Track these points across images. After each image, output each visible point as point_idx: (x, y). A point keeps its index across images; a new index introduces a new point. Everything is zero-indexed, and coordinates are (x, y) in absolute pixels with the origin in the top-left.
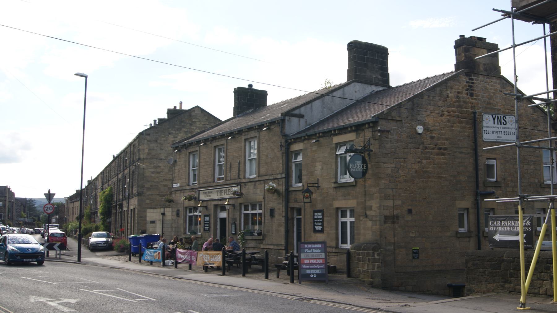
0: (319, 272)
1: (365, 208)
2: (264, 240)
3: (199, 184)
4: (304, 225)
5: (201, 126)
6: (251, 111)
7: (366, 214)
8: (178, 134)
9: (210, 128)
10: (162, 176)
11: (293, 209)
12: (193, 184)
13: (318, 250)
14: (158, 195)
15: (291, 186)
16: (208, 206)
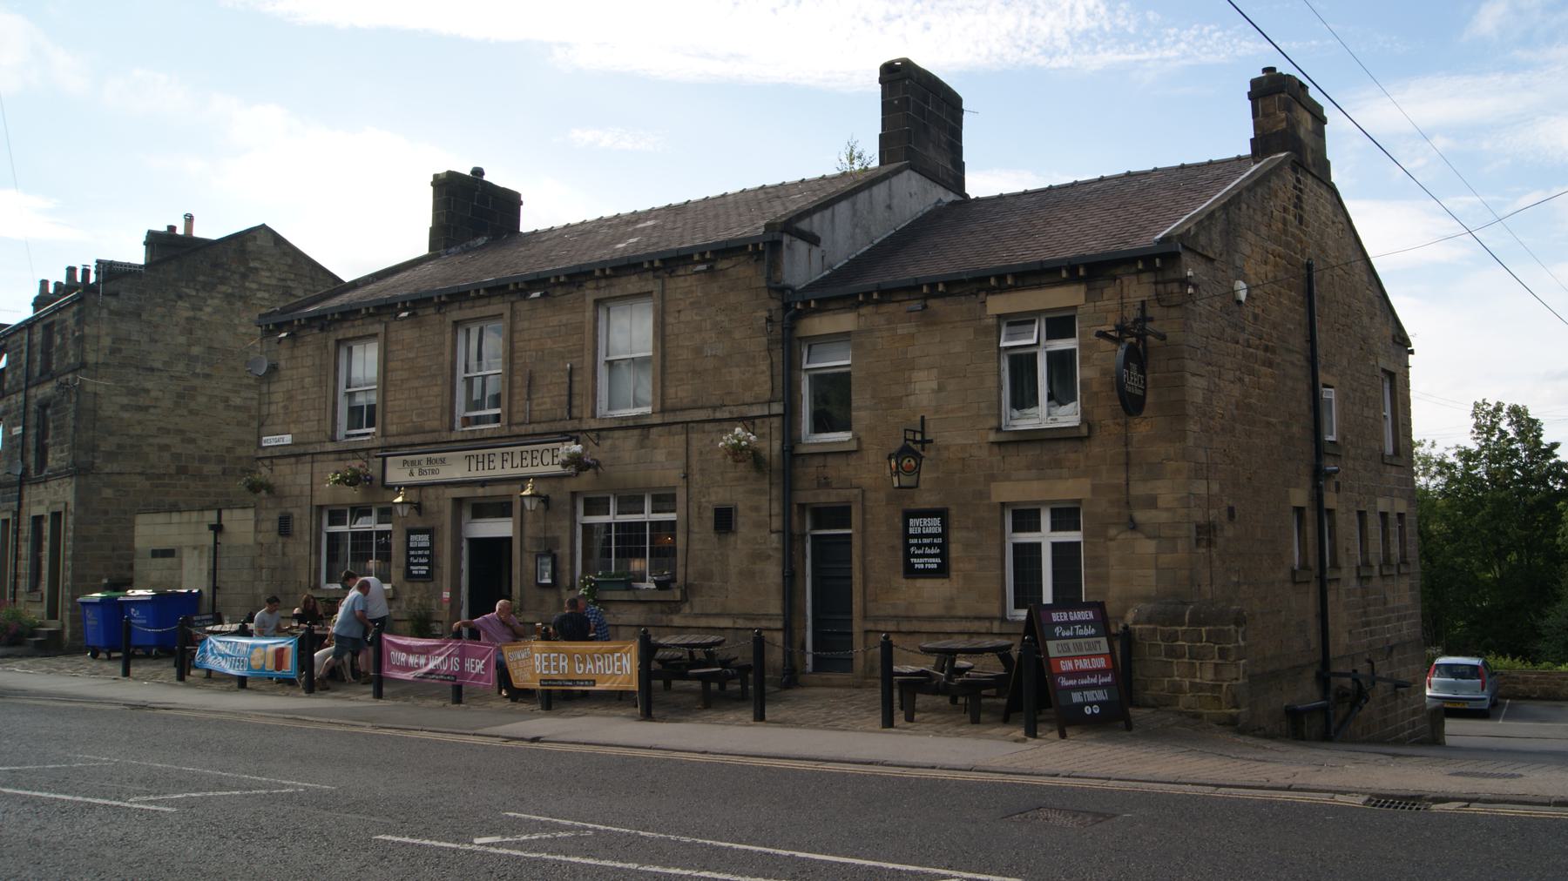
0: (1104, 698)
1: (1128, 503)
2: (687, 601)
3: (384, 435)
4: (864, 556)
5: (274, 282)
6: (481, 241)
7: (1131, 519)
8: (205, 300)
9: (371, 279)
10: (153, 418)
11: (802, 507)
12: (348, 436)
13: (1087, 628)
14: (141, 474)
15: (799, 441)
16: (427, 504)
